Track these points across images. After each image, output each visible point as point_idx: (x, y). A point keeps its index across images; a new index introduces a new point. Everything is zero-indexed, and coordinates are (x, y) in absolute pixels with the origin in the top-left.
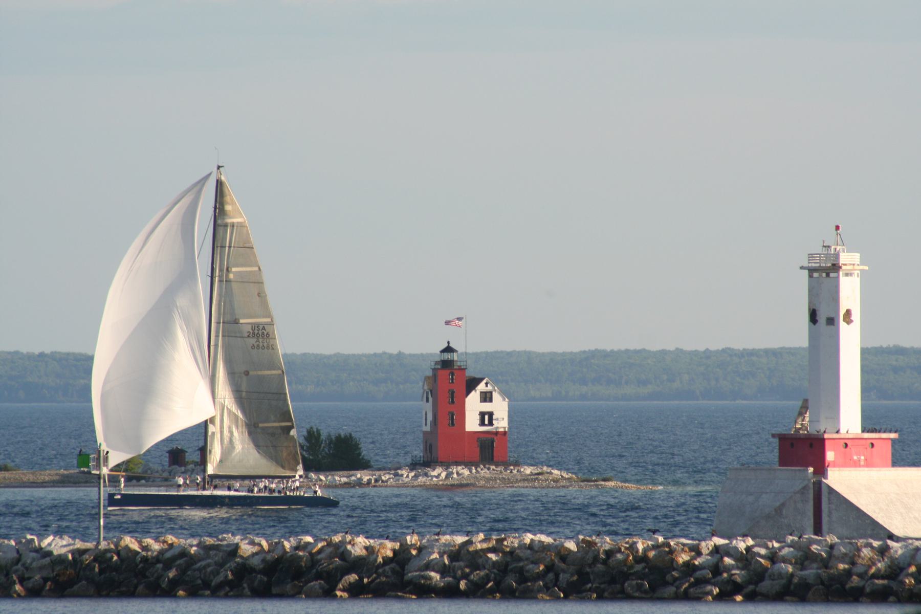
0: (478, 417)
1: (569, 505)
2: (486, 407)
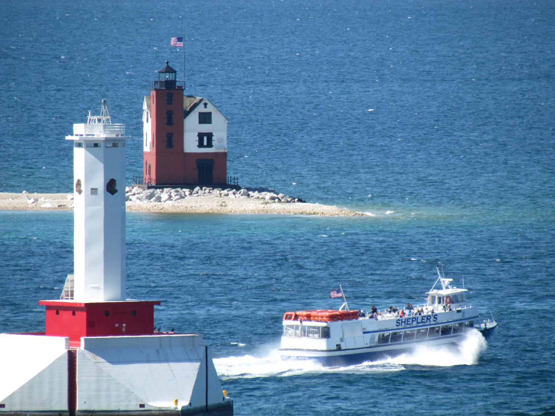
0: (197, 138)
1: (233, 100)
2: (205, 128)
